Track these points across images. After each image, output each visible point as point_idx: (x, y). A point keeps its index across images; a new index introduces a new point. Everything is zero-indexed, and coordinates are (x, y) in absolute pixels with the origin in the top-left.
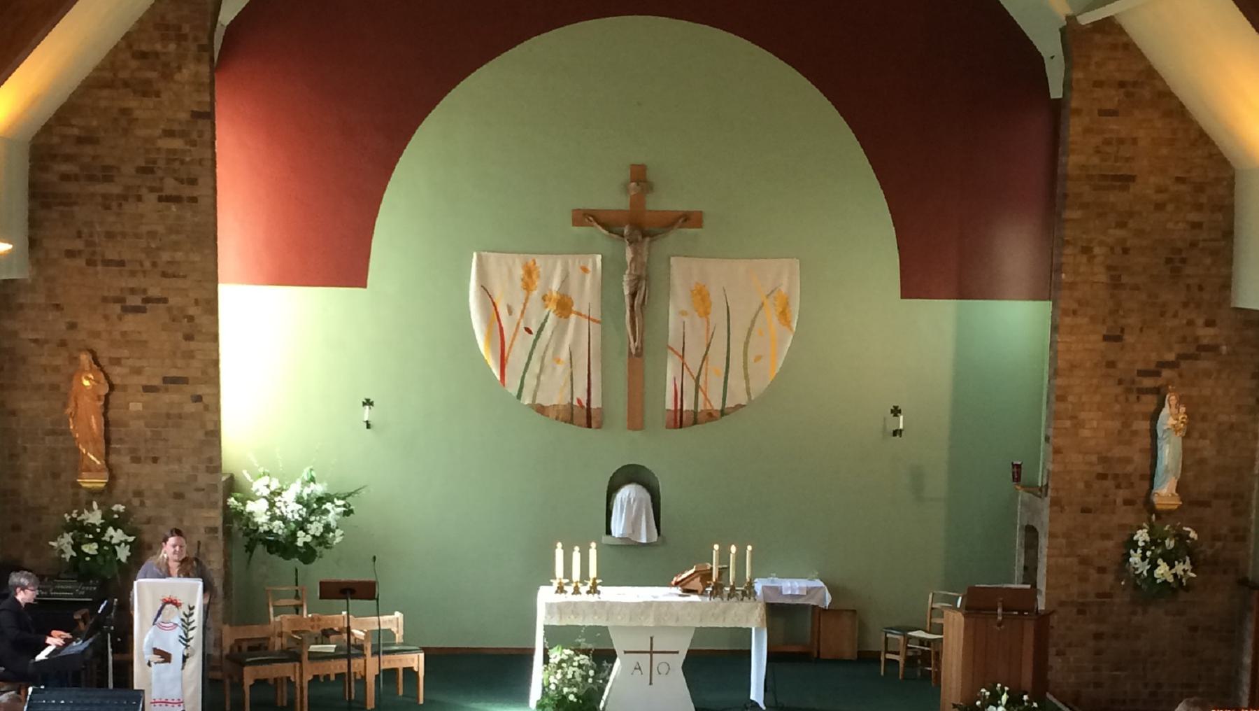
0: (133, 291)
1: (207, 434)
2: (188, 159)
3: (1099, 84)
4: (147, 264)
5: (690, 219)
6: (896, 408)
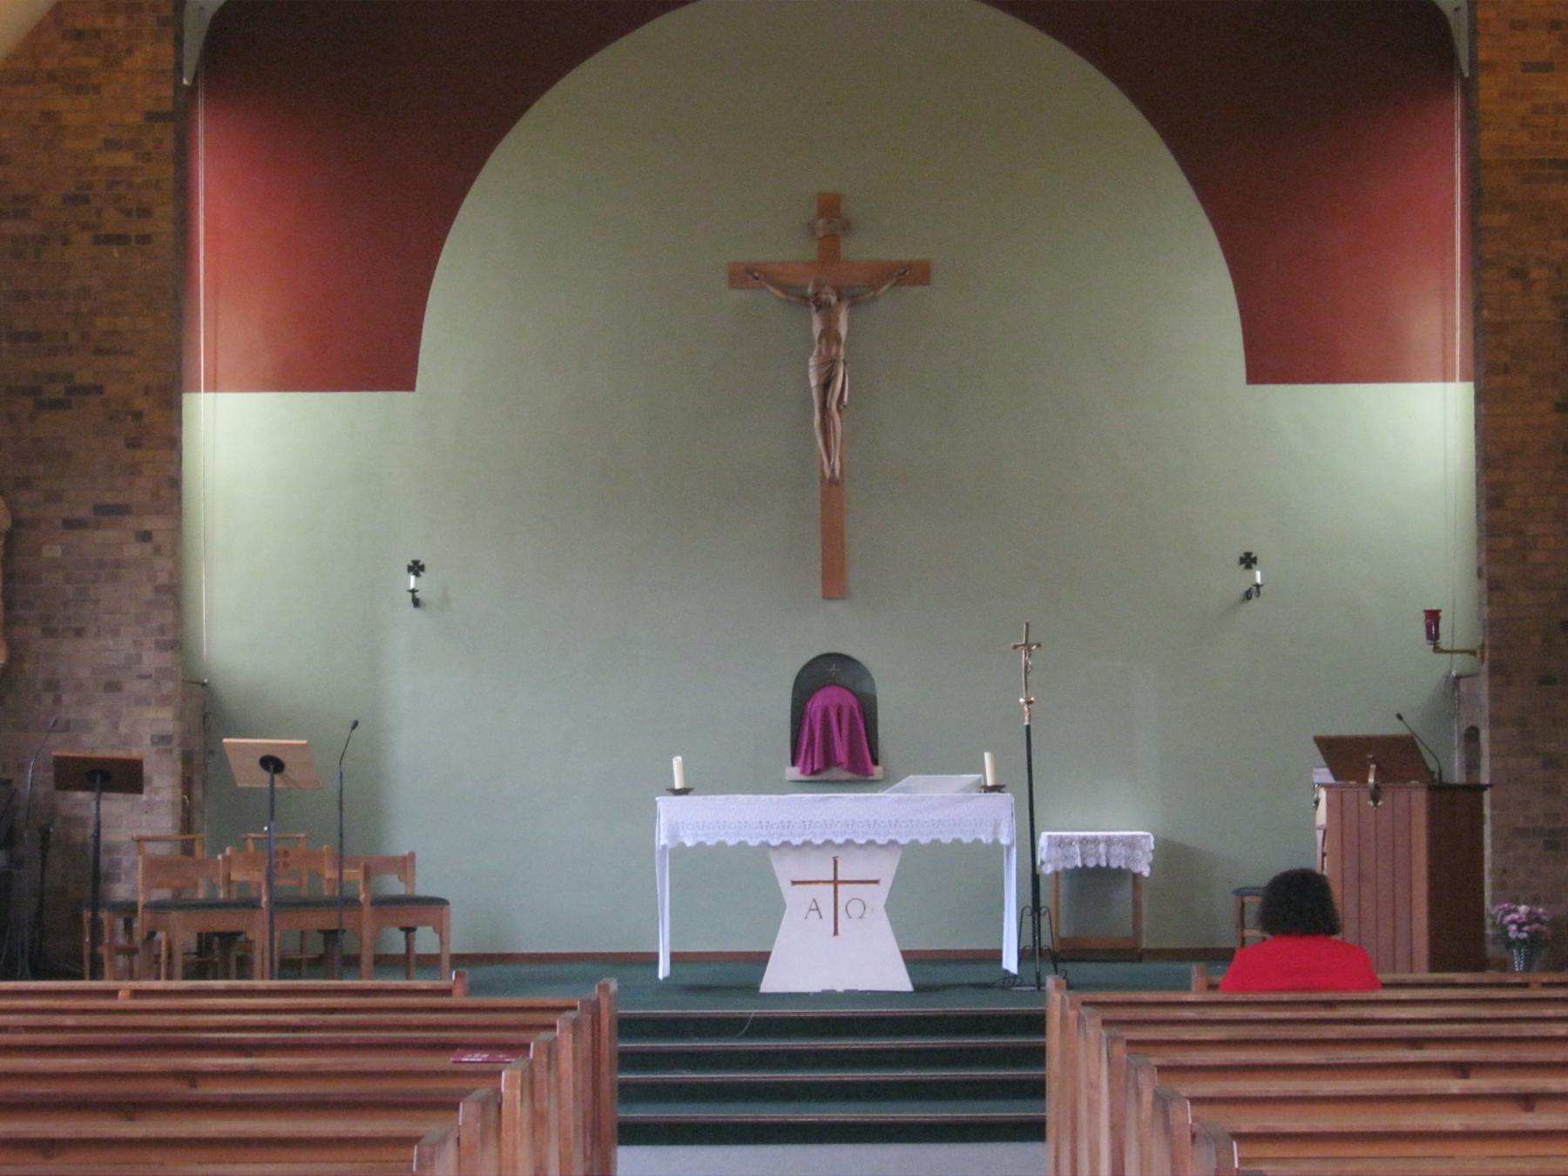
0: (52, 378)
1: (159, 589)
2: (139, 180)
3: (1520, 26)
4: (74, 338)
5: (914, 274)
6: (1248, 555)
